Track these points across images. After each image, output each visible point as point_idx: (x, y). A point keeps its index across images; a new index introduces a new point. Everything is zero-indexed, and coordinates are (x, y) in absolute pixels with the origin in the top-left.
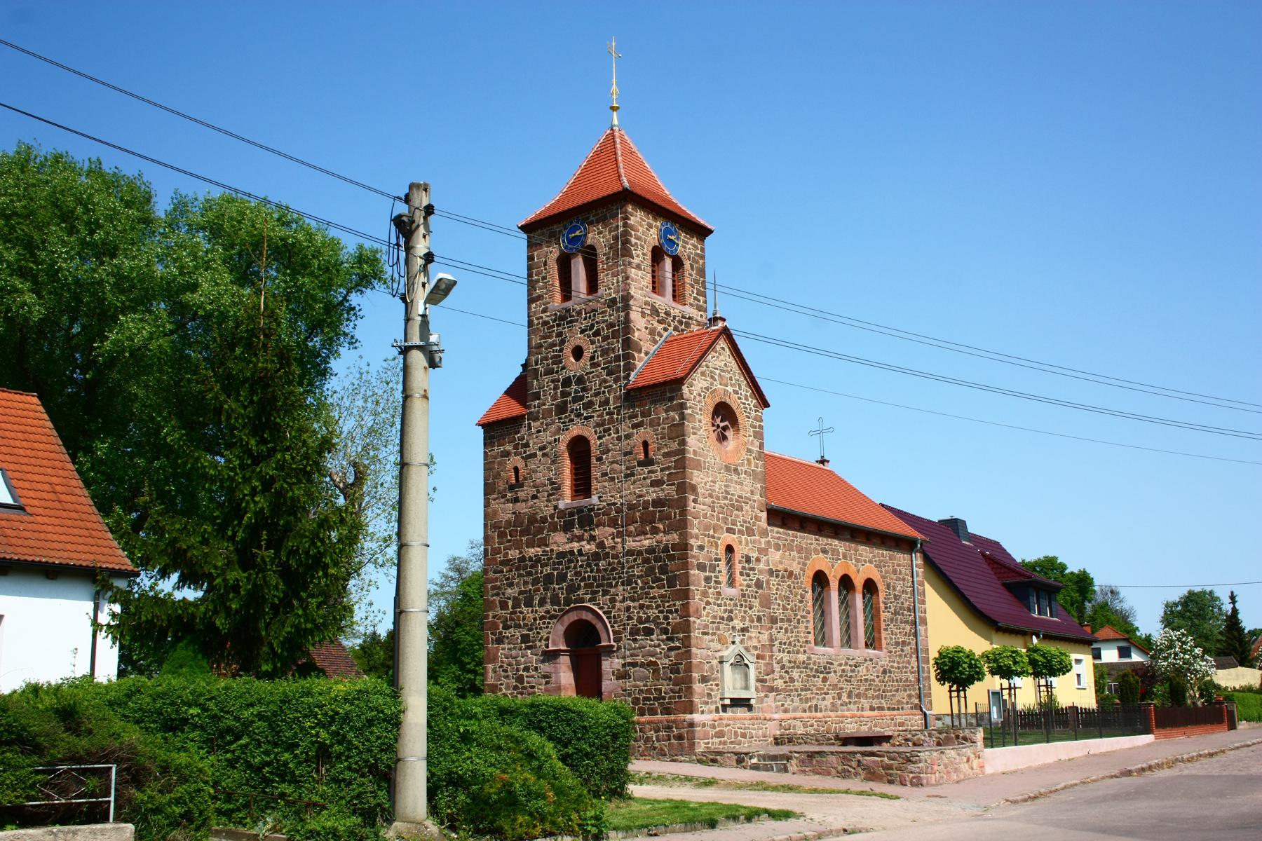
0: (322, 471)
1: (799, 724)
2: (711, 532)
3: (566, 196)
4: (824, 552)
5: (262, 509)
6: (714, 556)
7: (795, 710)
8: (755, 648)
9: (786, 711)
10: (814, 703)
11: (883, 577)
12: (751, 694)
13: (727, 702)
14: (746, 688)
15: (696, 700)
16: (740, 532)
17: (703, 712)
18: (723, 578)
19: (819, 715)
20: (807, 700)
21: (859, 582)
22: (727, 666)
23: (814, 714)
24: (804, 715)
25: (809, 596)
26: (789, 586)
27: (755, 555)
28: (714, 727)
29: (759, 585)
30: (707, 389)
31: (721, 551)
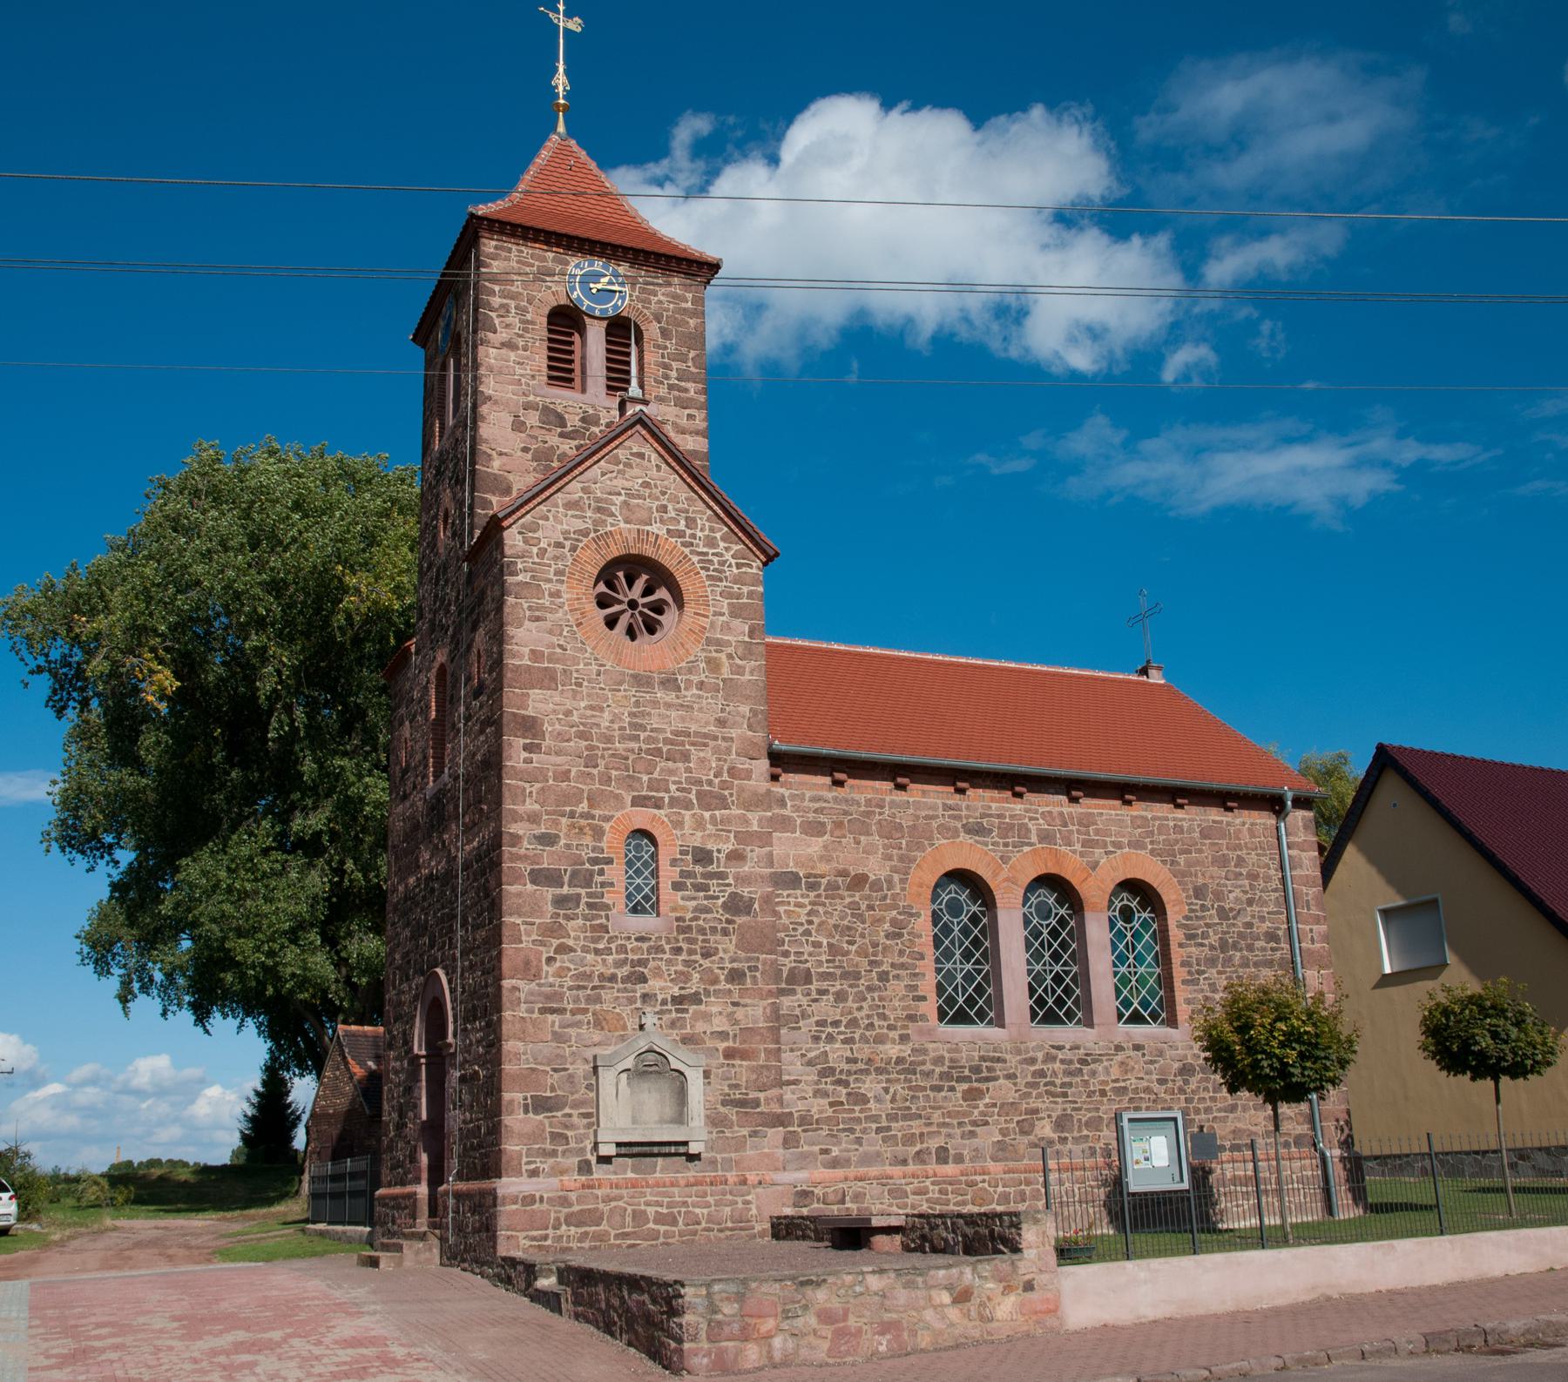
0: (136, 848)
1: (875, 1189)
2: (584, 807)
3: (1401, 750)
4: (977, 830)
5: (1477, 1043)
6: (586, 854)
7: (867, 1160)
8: (723, 1035)
9: (835, 1164)
10: (933, 1144)
11: (1181, 875)
12: (697, 1135)
13: (607, 1150)
14: (680, 1118)
15: (511, 1147)
16: (674, 802)
17: (534, 1173)
18: (616, 898)
19: (950, 1169)
20: (909, 1140)
21: (1096, 888)
22: (607, 1077)
23: (932, 1167)
24: (897, 1171)
25: (923, 927)
26: (854, 906)
27: (728, 847)
28: (564, 1202)
29: (737, 905)
30: (585, 533)
31: (613, 842)
